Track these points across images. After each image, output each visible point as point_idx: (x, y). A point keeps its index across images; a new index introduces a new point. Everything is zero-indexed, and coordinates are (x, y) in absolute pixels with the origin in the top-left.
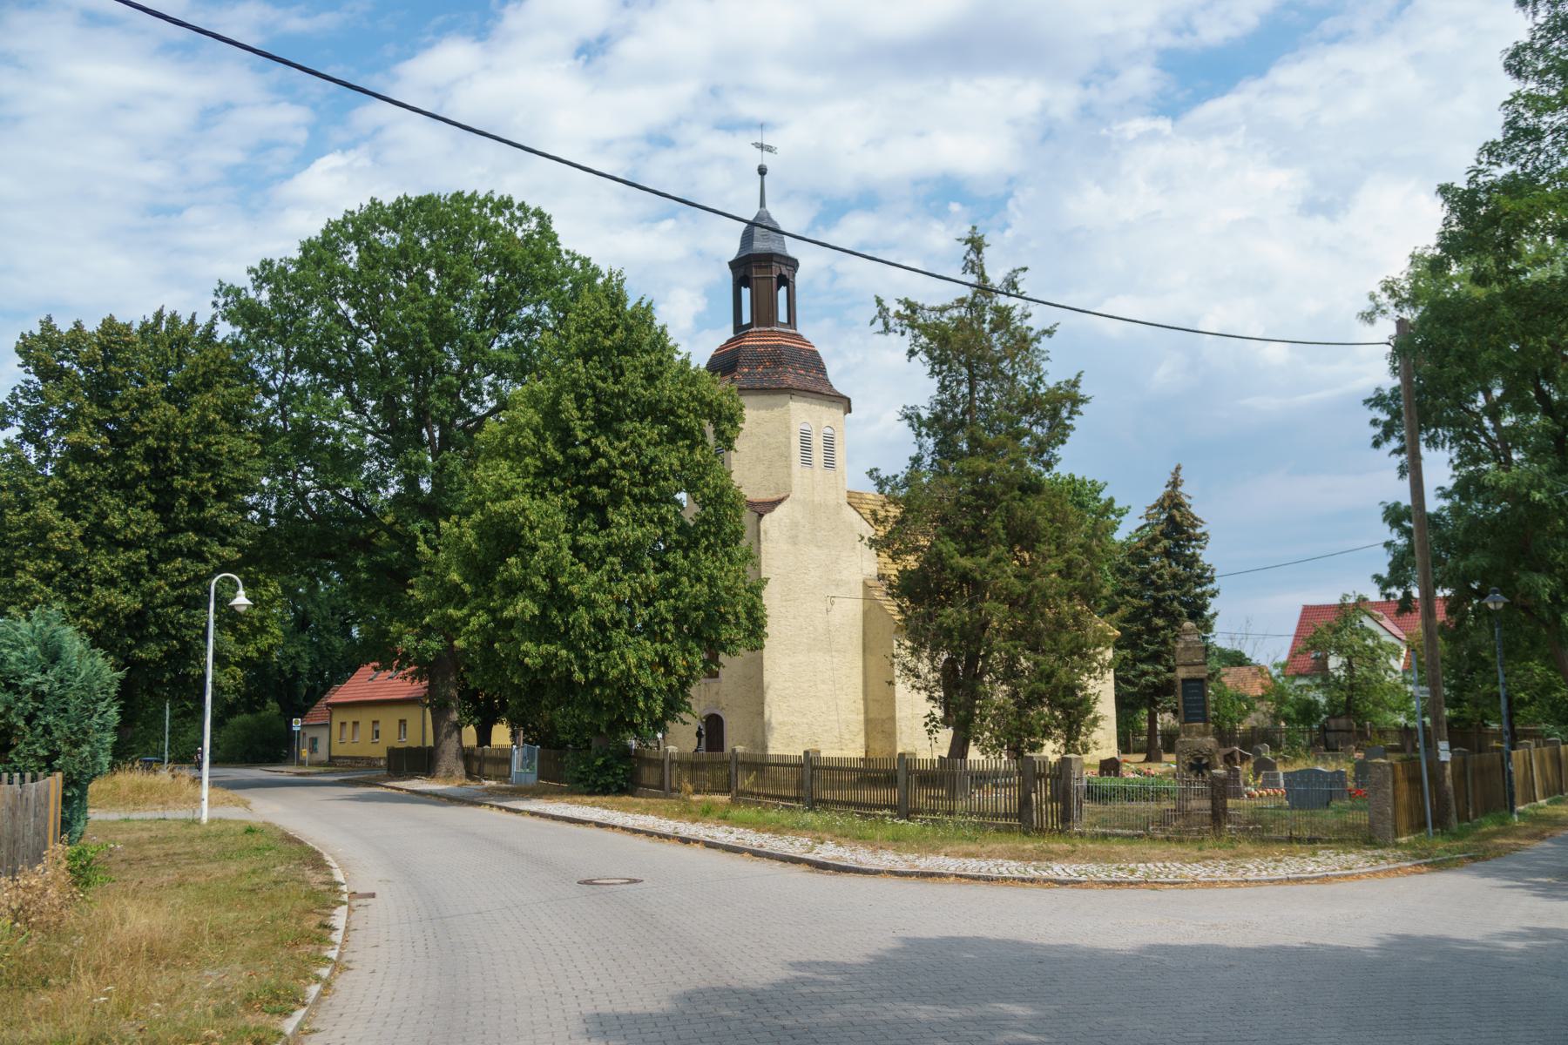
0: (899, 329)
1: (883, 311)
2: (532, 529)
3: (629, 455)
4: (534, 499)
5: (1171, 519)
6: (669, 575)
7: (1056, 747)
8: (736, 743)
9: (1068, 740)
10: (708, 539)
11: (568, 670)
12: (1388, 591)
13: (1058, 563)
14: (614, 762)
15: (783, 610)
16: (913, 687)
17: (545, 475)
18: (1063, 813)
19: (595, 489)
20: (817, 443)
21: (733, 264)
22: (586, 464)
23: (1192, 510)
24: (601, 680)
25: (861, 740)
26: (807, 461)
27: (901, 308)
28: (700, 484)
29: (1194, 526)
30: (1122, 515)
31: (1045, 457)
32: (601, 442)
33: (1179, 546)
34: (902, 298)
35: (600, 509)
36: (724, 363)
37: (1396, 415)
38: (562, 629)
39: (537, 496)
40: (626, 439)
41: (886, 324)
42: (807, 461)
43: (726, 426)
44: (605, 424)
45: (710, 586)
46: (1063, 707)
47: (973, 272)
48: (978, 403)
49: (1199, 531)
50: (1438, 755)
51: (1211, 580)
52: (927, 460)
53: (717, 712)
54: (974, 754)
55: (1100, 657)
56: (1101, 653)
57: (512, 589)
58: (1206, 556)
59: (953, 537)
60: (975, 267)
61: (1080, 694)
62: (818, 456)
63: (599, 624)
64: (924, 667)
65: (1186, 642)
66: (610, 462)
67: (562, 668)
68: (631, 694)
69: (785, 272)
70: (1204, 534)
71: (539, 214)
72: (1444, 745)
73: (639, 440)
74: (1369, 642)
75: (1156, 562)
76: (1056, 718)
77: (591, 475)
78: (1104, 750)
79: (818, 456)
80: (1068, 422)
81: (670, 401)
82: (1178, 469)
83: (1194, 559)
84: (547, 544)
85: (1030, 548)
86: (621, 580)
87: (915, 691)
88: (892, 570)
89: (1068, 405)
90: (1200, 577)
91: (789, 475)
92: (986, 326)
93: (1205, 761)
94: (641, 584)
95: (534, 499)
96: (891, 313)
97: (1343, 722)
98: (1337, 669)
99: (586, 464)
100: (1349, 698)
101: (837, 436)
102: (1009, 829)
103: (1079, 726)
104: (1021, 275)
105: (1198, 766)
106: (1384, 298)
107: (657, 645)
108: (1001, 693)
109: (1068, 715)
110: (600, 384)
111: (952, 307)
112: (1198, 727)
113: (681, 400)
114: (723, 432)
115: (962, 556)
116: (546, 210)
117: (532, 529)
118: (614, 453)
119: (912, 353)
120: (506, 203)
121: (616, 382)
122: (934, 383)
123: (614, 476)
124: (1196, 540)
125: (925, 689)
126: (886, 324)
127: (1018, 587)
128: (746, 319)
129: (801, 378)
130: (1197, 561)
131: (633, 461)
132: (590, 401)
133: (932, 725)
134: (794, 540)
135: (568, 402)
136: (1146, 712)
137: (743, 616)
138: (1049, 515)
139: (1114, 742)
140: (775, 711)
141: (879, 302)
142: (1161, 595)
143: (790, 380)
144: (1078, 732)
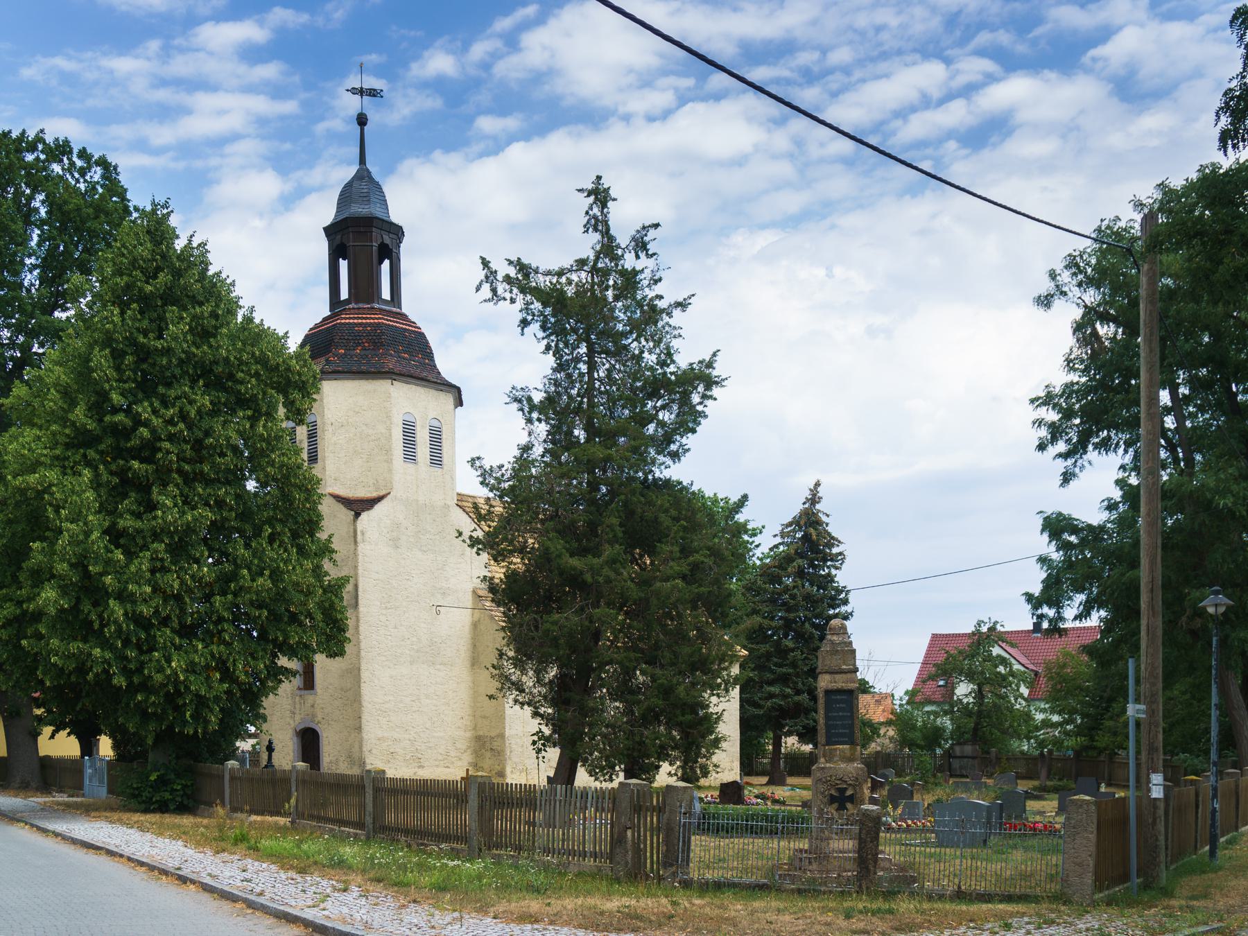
0: (508, 295)
1: (490, 276)
2: (57, 510)
3: (175, 425)
4: (65, 474)
5: (806, 537)
6: (228, 567)
7: (673, 769)
8: (332, 758)
9: (685, 762)
10: (273, 527)
11: (106, 671)
12: (1039, 612)
13: (683, 567)
14: (172, 776)
15: (383, 618)
16: (516, 701)
17: (79, 446)
18: (665, 856)
19: (136, 464)
20: (423, 437)
21: (329, 231)
22: (127, 433)
23: (829, 529)
24: (145, 686)
25: (467, 758)
26: (410, 454)
27: (512, 272)
28: (264, 461)
29: (831, 546)
30: (755, 535)
31: (673, 447)
32: (143, 410)
33: (814, 567)
34: (514, 258)
35: (144, 488)
36: (319, 341)
37: (1068, 414)
38: (96, 626)
39: (69, 471)
40: (173, 406)
41: (494, 291)
42: (410, 454)
43: (296, 395)
44: (145, 388)
45: (275, 582)
46: (680, 726)
47: (596, 230)
48: (597, 384)
49: (835, 550)
50: (1149, 790)
51: (846, 602)
52: (538, 450)
53: (312, 726)
54: (583, 778)
55: (725, 673)
56: (726, 669)
57: (40, 577)
58: (842, 578)
59: (561, 533)
60: (599, 224)
61: (701, 713)
62: (423, 450)
63: (138, 620)
64: (528, 680)
65: (832, 642)
66: (153, 431)
67: (97, 669)
68: (181, 702)
69: (387, 240)
70: (841, 554)
71: (103, 163)
72: (1157, 778)
73: (188, 407)
74: (1001, 669)
75: (789, 581)
76: (673, 738)
77: (132, 448)
78: (726, 772)
79: (423, 450)
80: (699, 408)
81: (227, 360)
82: (817, 484)
83: (830, 578)
84: (73, 526)
85: (652, 552)
86: (169, 570)
87: (517, 707)
88: (498, 573)
89: (701, 388)
90: (833, 598)
91: (390, 471)
92: (610, 294)
93: (849, 793)
94: (192, 577)
95: (65, 474)
96: (500, 277)
97: (968, 749)
98: (966, 696)
99: (127, 433)
100: (977, 724)
101: (444, 430)
102: (596, 875)
103: (699, 748)
104: (652, 234)
105: (841, 798)
106: (1065, 277)
107: (214, 648)
108: (614, 708)
109: (685, 735)
110: (141, 339)
111: (570, 271)
112: (842, 751)
113: (241, 362)
114: (293, 402)
115: (572, 555)
116: (112, 159)
117: (57, 510)
118: (156, 421)
119: (524, 323)
120: (63, 146)
121: (160, 337)
122: (550, 360)
123: (160, 449)
124: (832, 560)
125: (529, 704)
126: (494, 291)
127: (635, 592)
128: (344, 295)
129: (404, 362)
130: (833, 581)
131: (181, 431)
132: (129, 359)
133: (541, 743)
134: (395, 543)
135: (101, 358)
136: (771, 735)
137: (319, 617)
138: (673, 513)
139: (737, 765)
140: (373, 729)
141: (485, 263)
142: (792, 615)
143: (391, 364)
144: (698, 755)
